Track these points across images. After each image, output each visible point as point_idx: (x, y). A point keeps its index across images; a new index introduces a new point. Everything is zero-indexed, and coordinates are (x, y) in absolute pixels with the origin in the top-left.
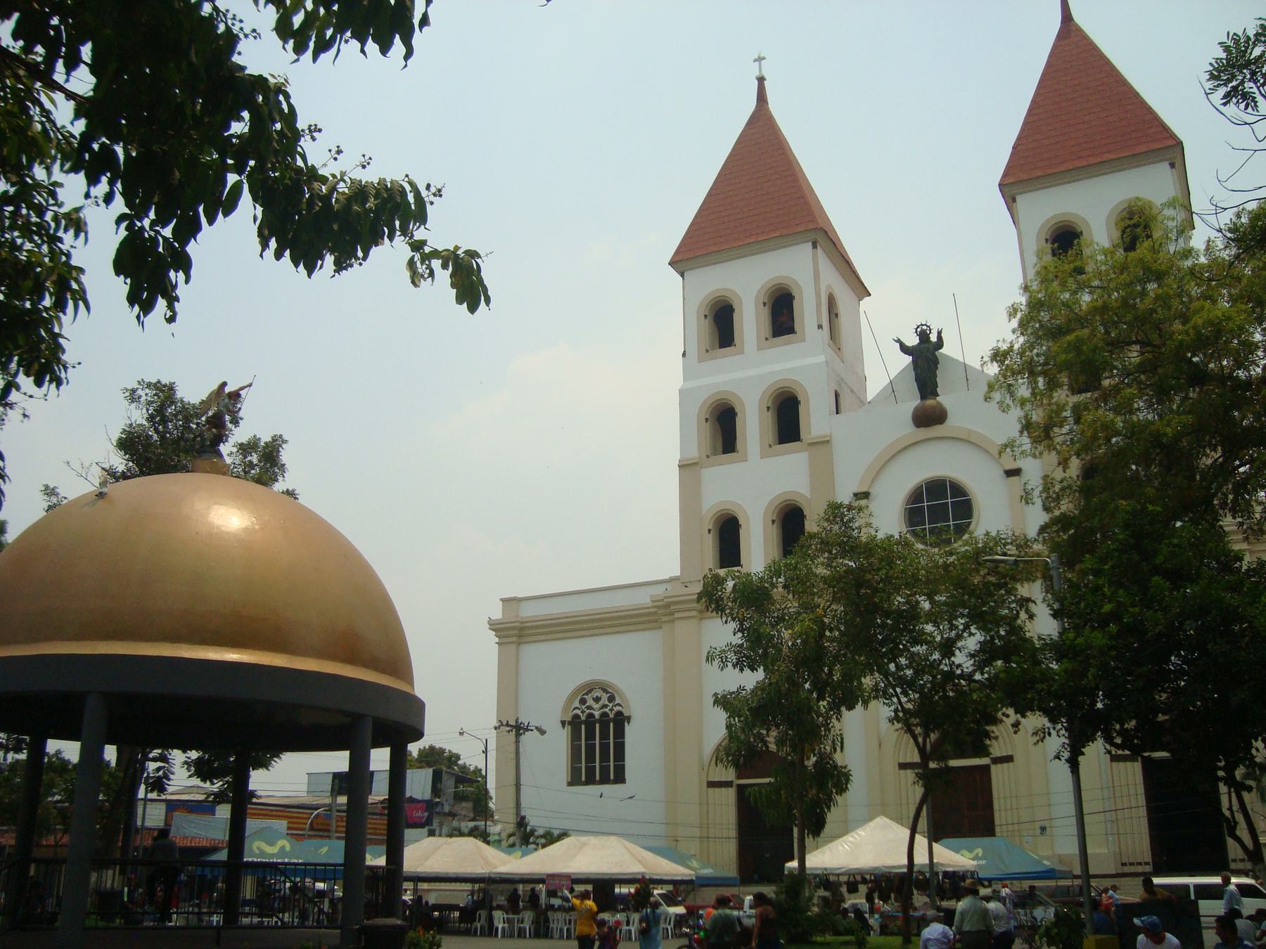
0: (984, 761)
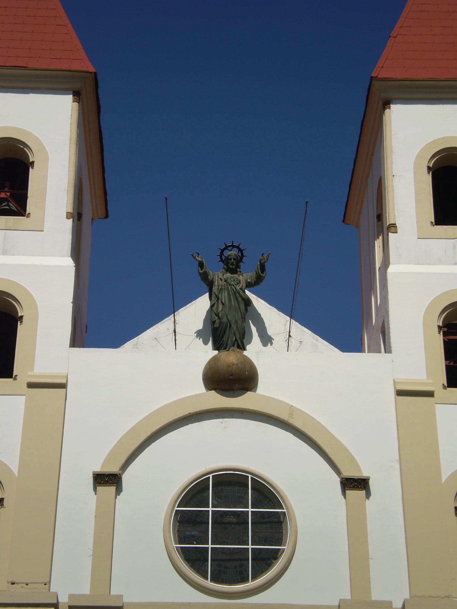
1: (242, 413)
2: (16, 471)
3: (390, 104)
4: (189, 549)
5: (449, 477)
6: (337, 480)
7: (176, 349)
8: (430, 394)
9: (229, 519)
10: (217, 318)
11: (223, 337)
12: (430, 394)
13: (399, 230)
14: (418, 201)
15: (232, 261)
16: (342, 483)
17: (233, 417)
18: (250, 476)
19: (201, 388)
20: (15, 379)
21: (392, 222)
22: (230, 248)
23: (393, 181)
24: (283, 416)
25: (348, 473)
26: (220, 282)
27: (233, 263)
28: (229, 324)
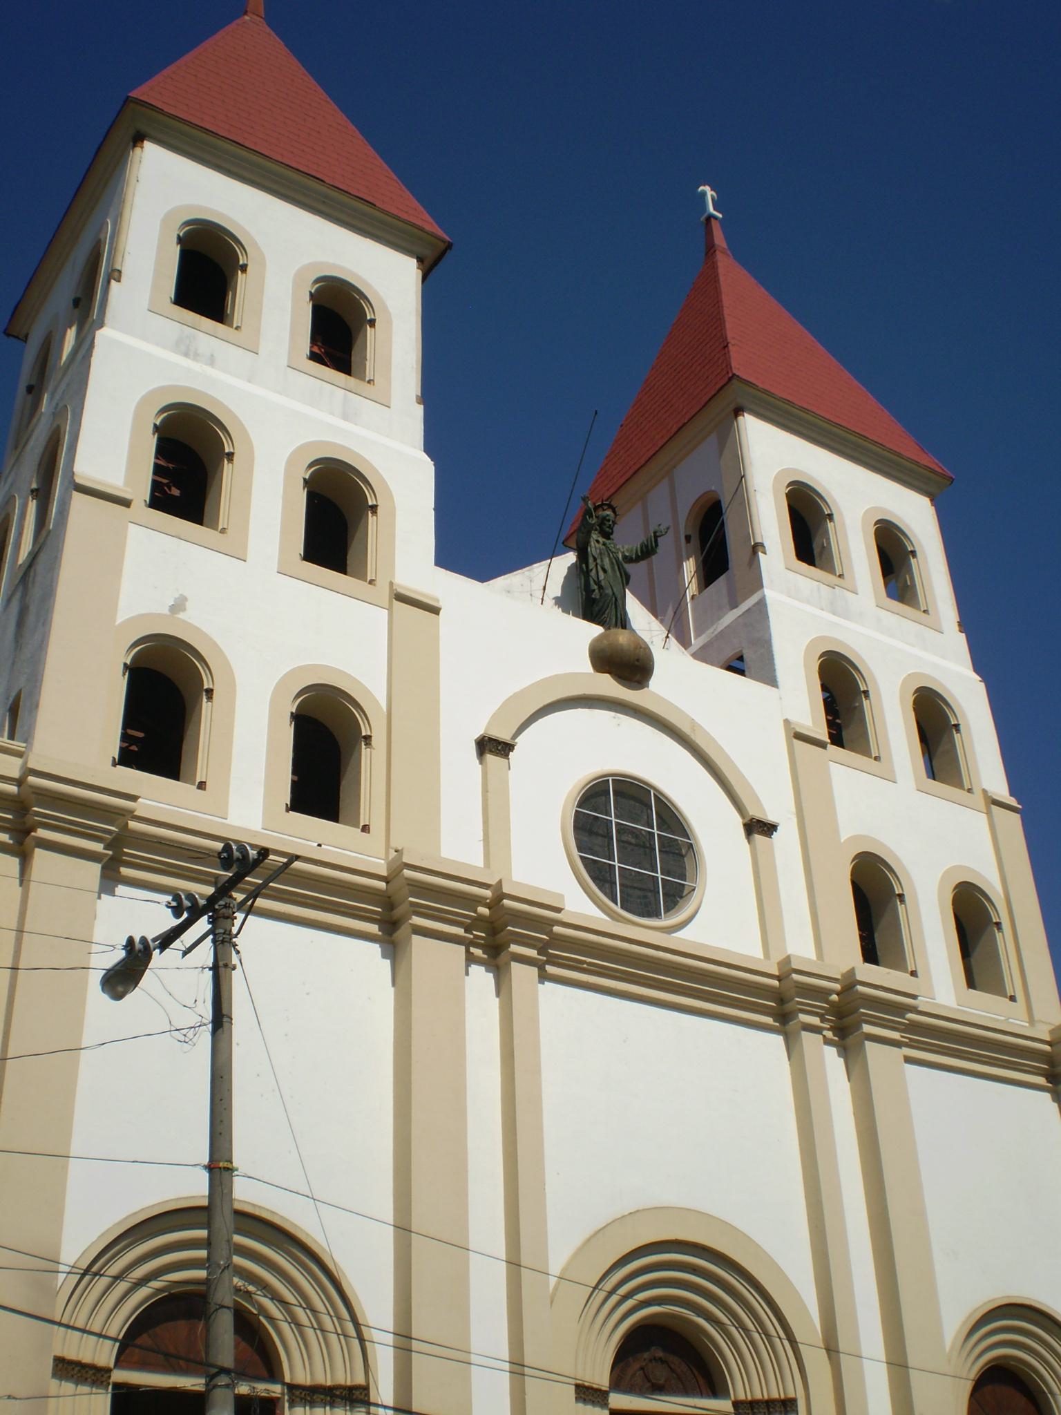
0: (119, 1376)
1: (636, 713)
2: (117, 623)
3: (743, 411)
4: (864, 944)
5: (125, 621)
6: (737, 822)
7: (542, 603)
8: (126, 503)
9: (627, 838)
10: (596, 587)
11: (604, 613)
12: (126, 503)
13: (123, 279)
14: (780, 528)
15: (611, 523)
16: (745, 825)
17: (626, 714)
18: (610, 779)
19: (586, 666)
20: (223, 531)
21: (759, 540)
22: (605, 507)
23: (755, 496)
24: (685, 728)
25: (754, 812)
26: (597, 545)
27: (610, 525)
28: (614, 599)
